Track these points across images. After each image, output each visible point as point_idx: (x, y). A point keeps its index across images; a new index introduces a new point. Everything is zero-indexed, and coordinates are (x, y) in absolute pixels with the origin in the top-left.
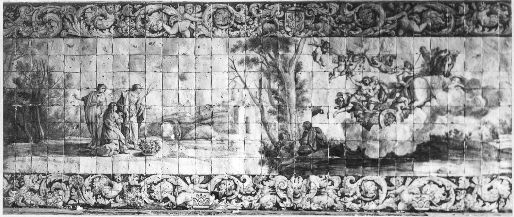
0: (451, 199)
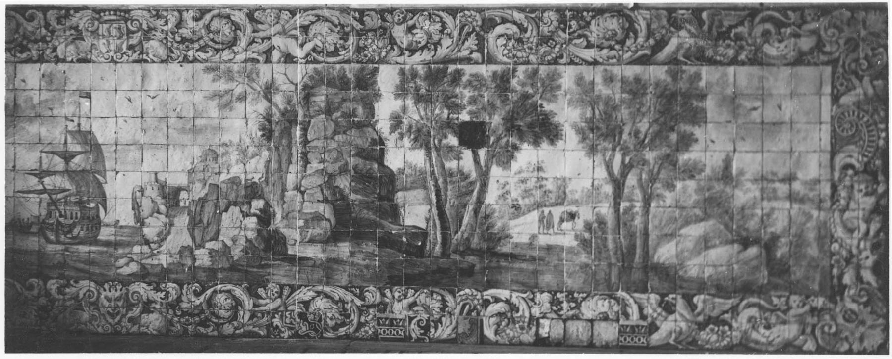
0: (352, 320)
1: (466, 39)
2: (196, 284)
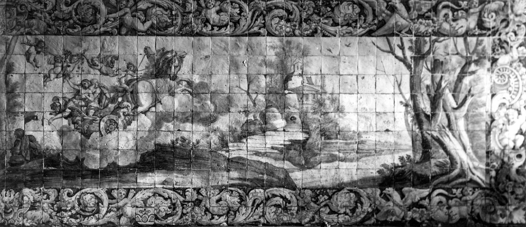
0: (177, 212)
1: (256, 20)
2: (70, 190)
